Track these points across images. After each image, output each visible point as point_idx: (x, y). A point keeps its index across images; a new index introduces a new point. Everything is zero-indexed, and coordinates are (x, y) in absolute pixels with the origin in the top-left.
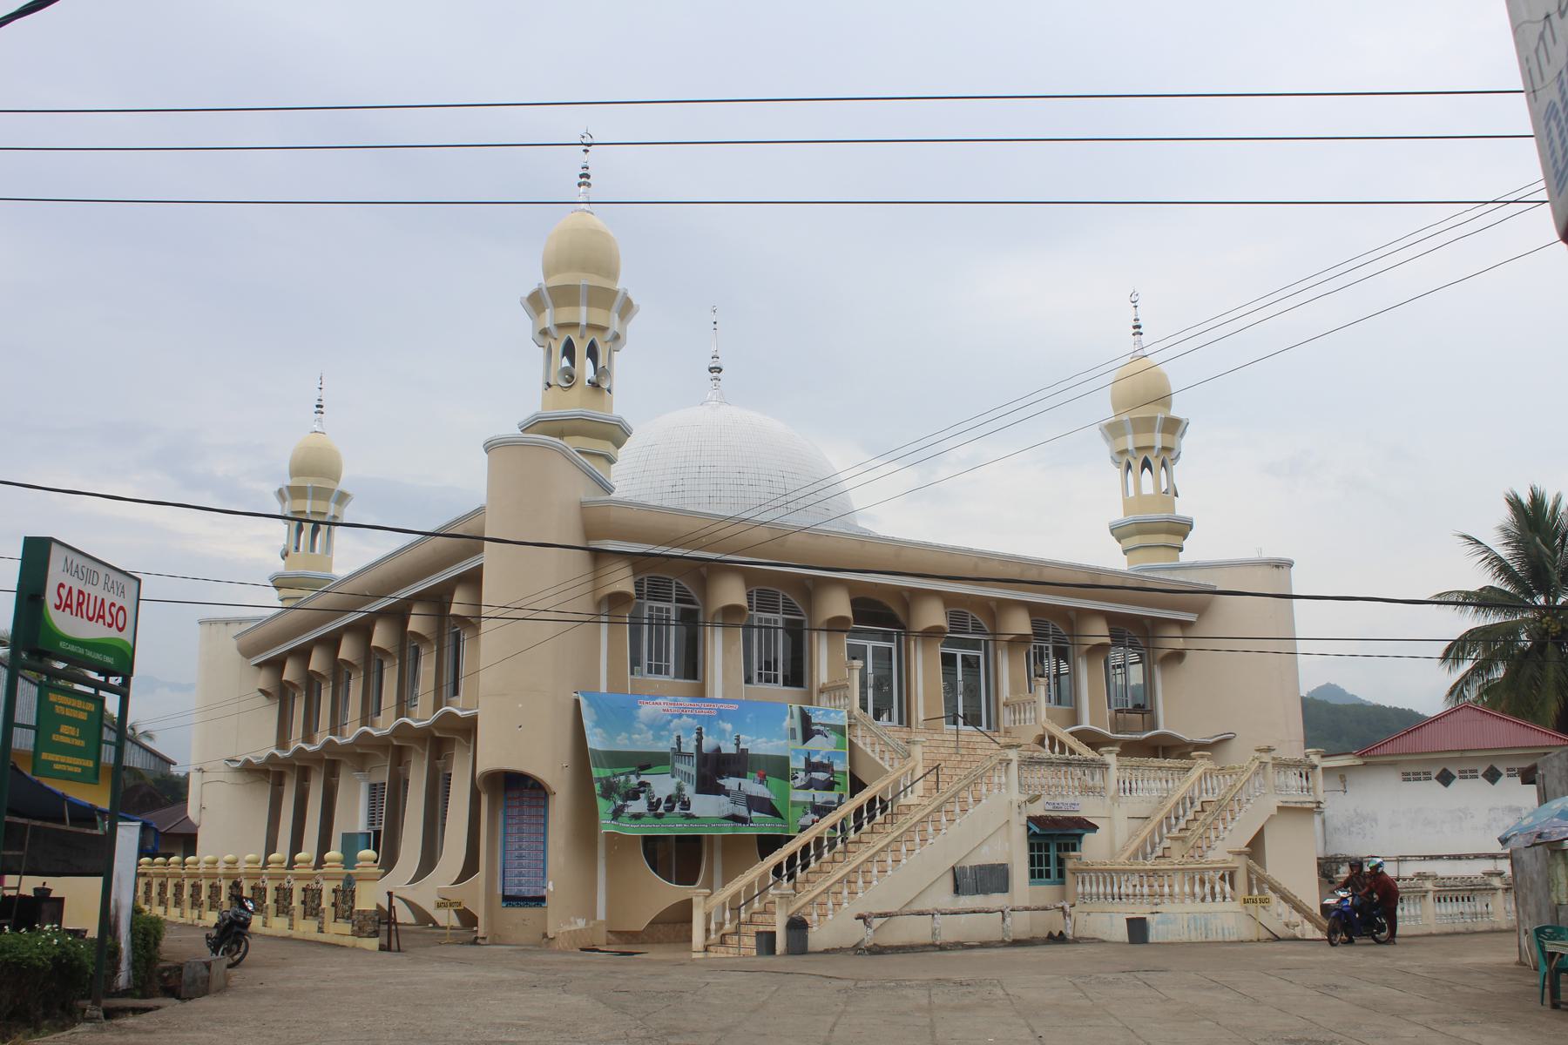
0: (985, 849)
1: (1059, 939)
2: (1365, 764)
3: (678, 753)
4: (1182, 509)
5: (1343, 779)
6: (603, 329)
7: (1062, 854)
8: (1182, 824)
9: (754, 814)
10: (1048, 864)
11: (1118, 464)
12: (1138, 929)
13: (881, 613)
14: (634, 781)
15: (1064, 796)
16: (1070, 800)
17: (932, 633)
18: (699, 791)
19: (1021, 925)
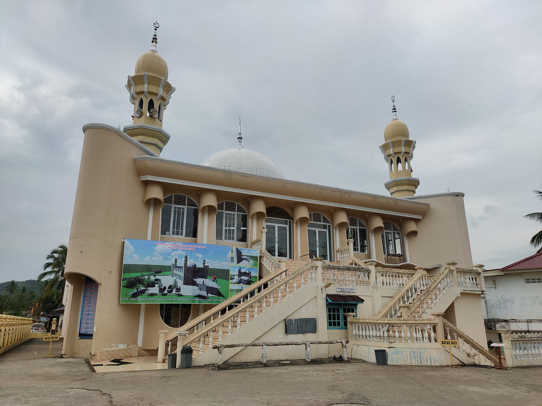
0: (303, 310)
1: (339, 360)
2: (506, 275)
3: (175, 266)
4: (414, 175)
5: (494, 282)
6: (156, 94)
7: (346, 314)
8: (411, 300)
9: (209, 295)
10: (338, 319)
11: (387, 160)
12: (381, 356)
13: (279, 211)
14: (152, 278)
15: (347, 285)
16: (350, 287)
17: (303, 220)
18: (186, 283)
19: (323, 351)
